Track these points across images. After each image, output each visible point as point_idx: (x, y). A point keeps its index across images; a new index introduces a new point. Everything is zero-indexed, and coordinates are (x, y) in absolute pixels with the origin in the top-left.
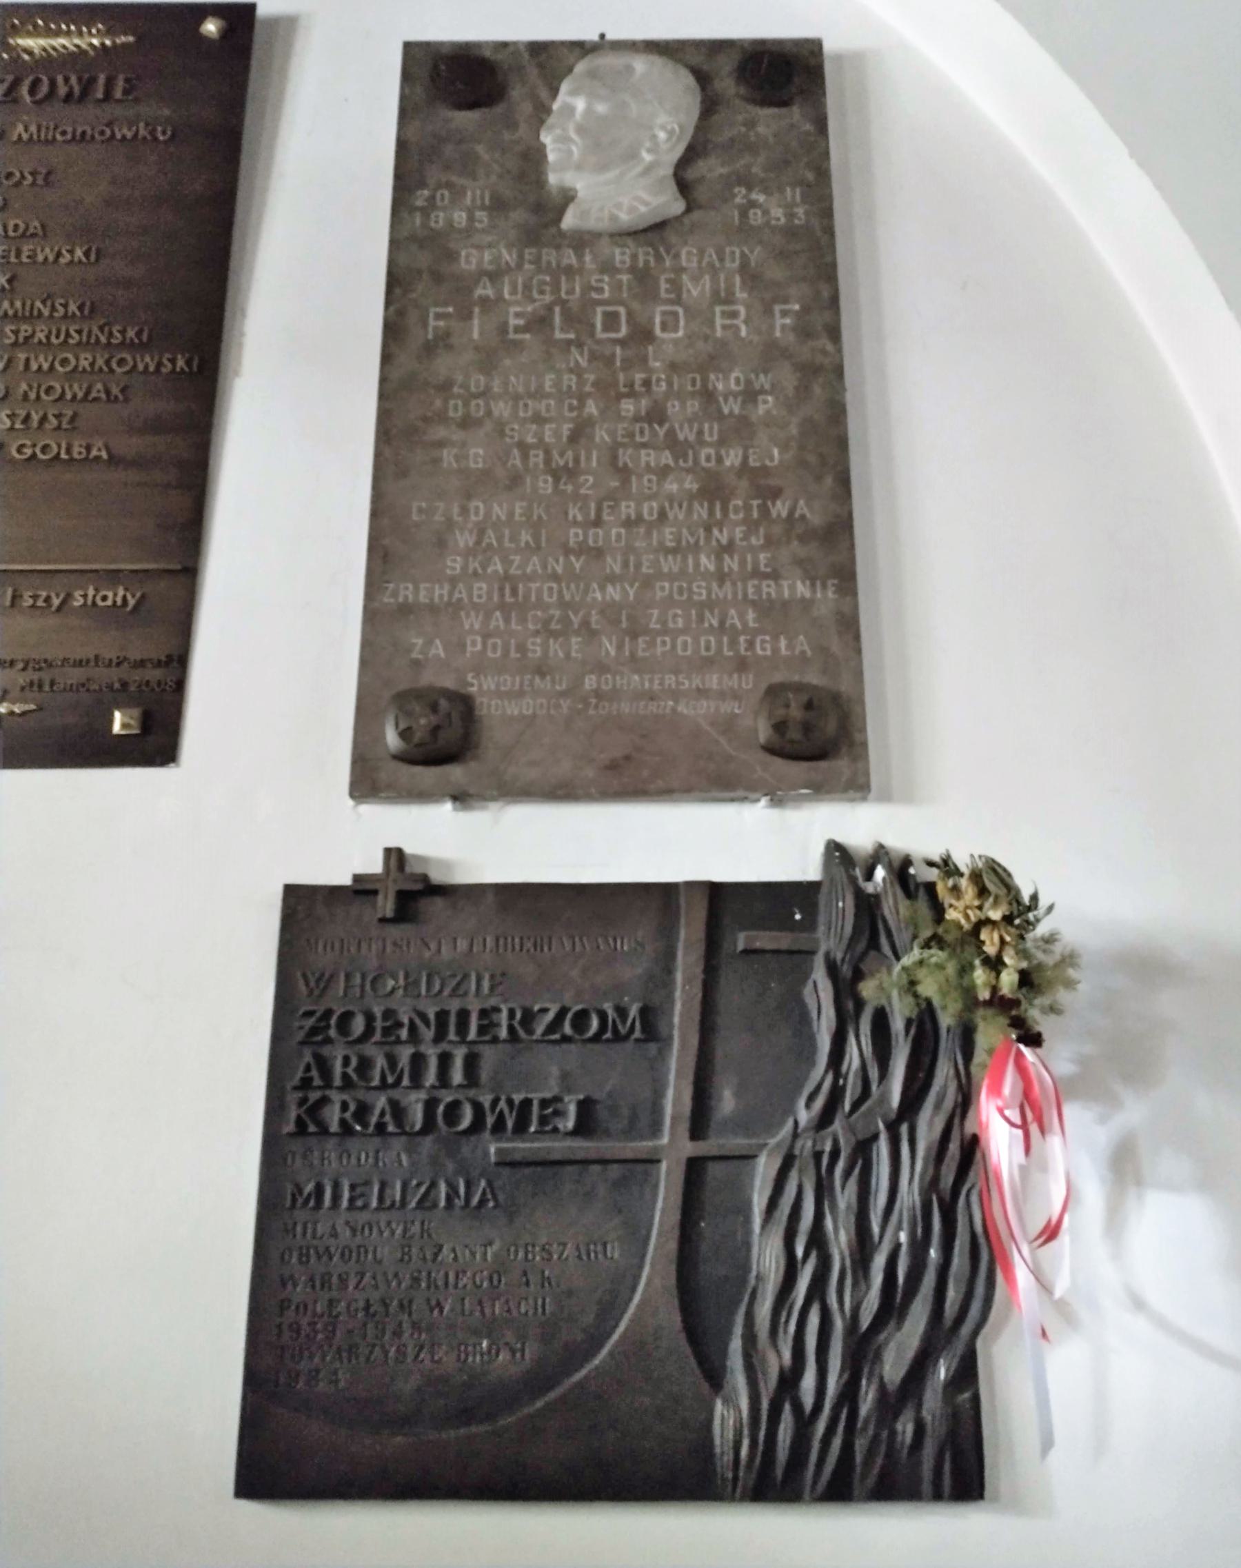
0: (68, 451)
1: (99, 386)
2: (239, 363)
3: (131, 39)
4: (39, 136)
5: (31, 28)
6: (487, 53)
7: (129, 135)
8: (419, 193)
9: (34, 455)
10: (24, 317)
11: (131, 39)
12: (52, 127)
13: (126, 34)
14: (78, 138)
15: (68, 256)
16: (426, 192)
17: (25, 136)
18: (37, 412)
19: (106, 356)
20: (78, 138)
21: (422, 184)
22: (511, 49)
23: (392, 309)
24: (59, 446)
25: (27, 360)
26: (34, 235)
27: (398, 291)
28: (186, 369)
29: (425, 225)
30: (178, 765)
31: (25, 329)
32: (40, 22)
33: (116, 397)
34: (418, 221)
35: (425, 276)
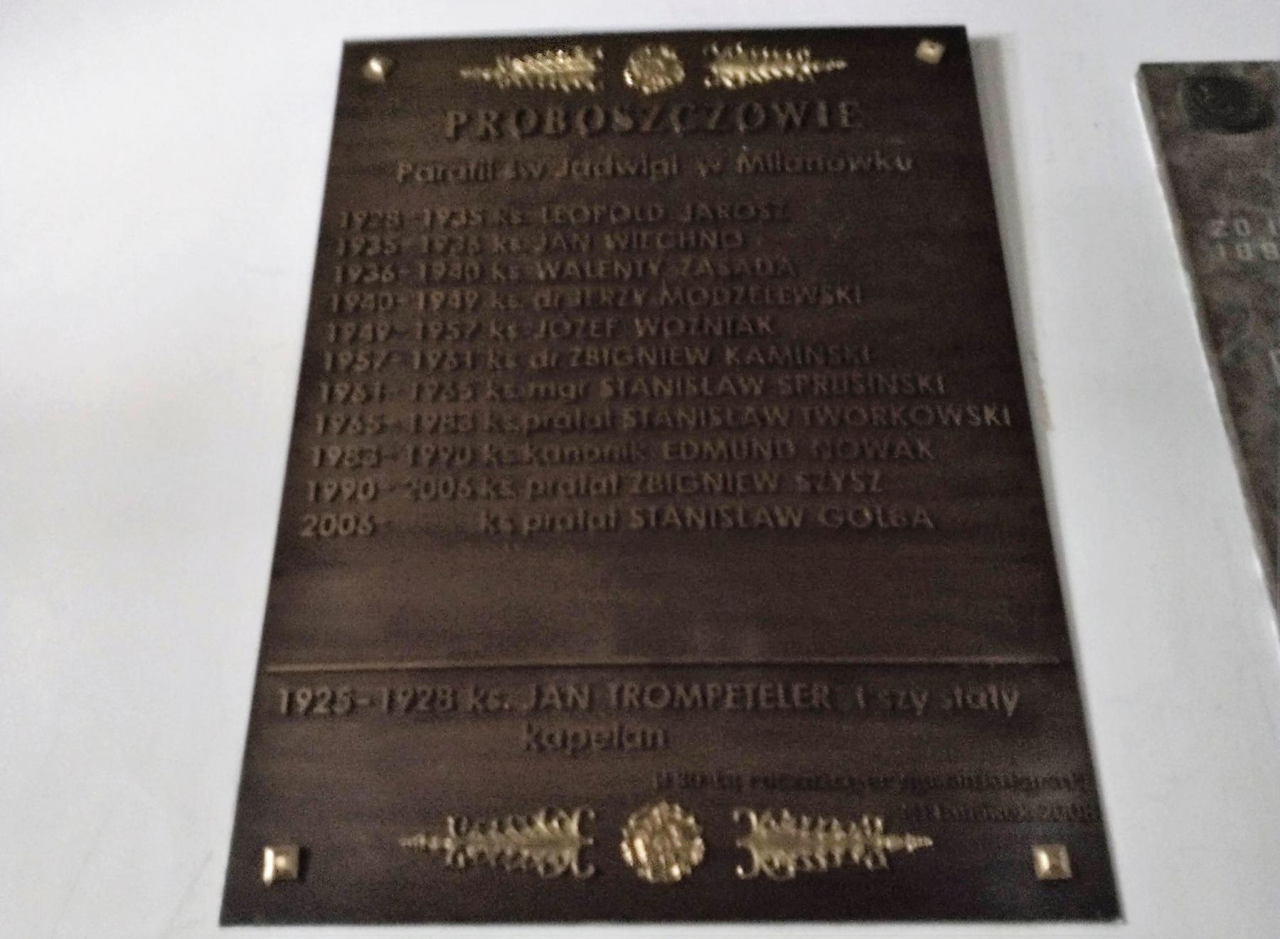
0: (885, 519)
1: (744, 319)
2: (1047, 414)
3: (841, 65)
4: (766, 167)
5: (730, 54)
6: (1239, 73)
7: (866, 167)
8: (1214, 223)
9: (846, 523)
10: (797, 367)
11: (841, 65)
12: (778, 157)
13: (836, 59)
14: (567, 458)
15: (375, 276)
16: (1222, 222)
17: (750, 168)
18: (838, 474)
19: (902, 408)
20: (567, 458)
21: (1215, 214)
22: (1263, 69)
23: (1226, 353)
24: (711, 293)
25: (812, 413)
26: (785, 274)
27: (1226, 332)
28: (998, 422)
29: (1232, 258)
30: (1125, 922)
31: (801, 377)
32: (739, 49)
33: (925, 455)
34: (1223, 253)
35: (1252, 314)
